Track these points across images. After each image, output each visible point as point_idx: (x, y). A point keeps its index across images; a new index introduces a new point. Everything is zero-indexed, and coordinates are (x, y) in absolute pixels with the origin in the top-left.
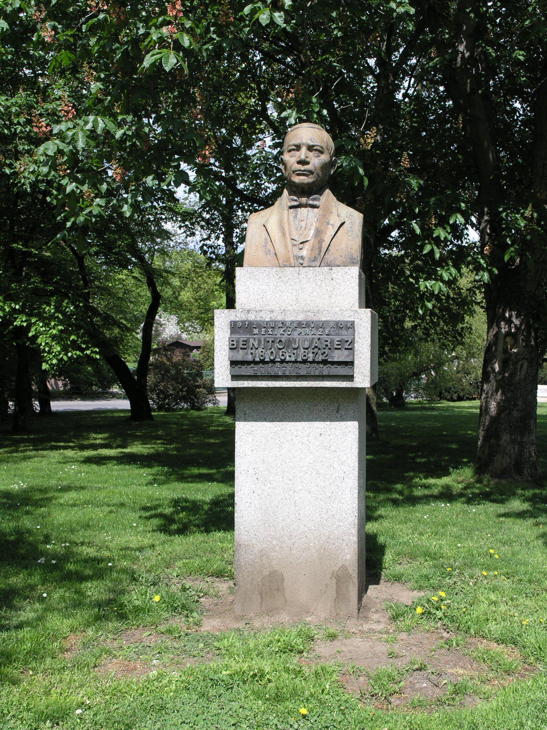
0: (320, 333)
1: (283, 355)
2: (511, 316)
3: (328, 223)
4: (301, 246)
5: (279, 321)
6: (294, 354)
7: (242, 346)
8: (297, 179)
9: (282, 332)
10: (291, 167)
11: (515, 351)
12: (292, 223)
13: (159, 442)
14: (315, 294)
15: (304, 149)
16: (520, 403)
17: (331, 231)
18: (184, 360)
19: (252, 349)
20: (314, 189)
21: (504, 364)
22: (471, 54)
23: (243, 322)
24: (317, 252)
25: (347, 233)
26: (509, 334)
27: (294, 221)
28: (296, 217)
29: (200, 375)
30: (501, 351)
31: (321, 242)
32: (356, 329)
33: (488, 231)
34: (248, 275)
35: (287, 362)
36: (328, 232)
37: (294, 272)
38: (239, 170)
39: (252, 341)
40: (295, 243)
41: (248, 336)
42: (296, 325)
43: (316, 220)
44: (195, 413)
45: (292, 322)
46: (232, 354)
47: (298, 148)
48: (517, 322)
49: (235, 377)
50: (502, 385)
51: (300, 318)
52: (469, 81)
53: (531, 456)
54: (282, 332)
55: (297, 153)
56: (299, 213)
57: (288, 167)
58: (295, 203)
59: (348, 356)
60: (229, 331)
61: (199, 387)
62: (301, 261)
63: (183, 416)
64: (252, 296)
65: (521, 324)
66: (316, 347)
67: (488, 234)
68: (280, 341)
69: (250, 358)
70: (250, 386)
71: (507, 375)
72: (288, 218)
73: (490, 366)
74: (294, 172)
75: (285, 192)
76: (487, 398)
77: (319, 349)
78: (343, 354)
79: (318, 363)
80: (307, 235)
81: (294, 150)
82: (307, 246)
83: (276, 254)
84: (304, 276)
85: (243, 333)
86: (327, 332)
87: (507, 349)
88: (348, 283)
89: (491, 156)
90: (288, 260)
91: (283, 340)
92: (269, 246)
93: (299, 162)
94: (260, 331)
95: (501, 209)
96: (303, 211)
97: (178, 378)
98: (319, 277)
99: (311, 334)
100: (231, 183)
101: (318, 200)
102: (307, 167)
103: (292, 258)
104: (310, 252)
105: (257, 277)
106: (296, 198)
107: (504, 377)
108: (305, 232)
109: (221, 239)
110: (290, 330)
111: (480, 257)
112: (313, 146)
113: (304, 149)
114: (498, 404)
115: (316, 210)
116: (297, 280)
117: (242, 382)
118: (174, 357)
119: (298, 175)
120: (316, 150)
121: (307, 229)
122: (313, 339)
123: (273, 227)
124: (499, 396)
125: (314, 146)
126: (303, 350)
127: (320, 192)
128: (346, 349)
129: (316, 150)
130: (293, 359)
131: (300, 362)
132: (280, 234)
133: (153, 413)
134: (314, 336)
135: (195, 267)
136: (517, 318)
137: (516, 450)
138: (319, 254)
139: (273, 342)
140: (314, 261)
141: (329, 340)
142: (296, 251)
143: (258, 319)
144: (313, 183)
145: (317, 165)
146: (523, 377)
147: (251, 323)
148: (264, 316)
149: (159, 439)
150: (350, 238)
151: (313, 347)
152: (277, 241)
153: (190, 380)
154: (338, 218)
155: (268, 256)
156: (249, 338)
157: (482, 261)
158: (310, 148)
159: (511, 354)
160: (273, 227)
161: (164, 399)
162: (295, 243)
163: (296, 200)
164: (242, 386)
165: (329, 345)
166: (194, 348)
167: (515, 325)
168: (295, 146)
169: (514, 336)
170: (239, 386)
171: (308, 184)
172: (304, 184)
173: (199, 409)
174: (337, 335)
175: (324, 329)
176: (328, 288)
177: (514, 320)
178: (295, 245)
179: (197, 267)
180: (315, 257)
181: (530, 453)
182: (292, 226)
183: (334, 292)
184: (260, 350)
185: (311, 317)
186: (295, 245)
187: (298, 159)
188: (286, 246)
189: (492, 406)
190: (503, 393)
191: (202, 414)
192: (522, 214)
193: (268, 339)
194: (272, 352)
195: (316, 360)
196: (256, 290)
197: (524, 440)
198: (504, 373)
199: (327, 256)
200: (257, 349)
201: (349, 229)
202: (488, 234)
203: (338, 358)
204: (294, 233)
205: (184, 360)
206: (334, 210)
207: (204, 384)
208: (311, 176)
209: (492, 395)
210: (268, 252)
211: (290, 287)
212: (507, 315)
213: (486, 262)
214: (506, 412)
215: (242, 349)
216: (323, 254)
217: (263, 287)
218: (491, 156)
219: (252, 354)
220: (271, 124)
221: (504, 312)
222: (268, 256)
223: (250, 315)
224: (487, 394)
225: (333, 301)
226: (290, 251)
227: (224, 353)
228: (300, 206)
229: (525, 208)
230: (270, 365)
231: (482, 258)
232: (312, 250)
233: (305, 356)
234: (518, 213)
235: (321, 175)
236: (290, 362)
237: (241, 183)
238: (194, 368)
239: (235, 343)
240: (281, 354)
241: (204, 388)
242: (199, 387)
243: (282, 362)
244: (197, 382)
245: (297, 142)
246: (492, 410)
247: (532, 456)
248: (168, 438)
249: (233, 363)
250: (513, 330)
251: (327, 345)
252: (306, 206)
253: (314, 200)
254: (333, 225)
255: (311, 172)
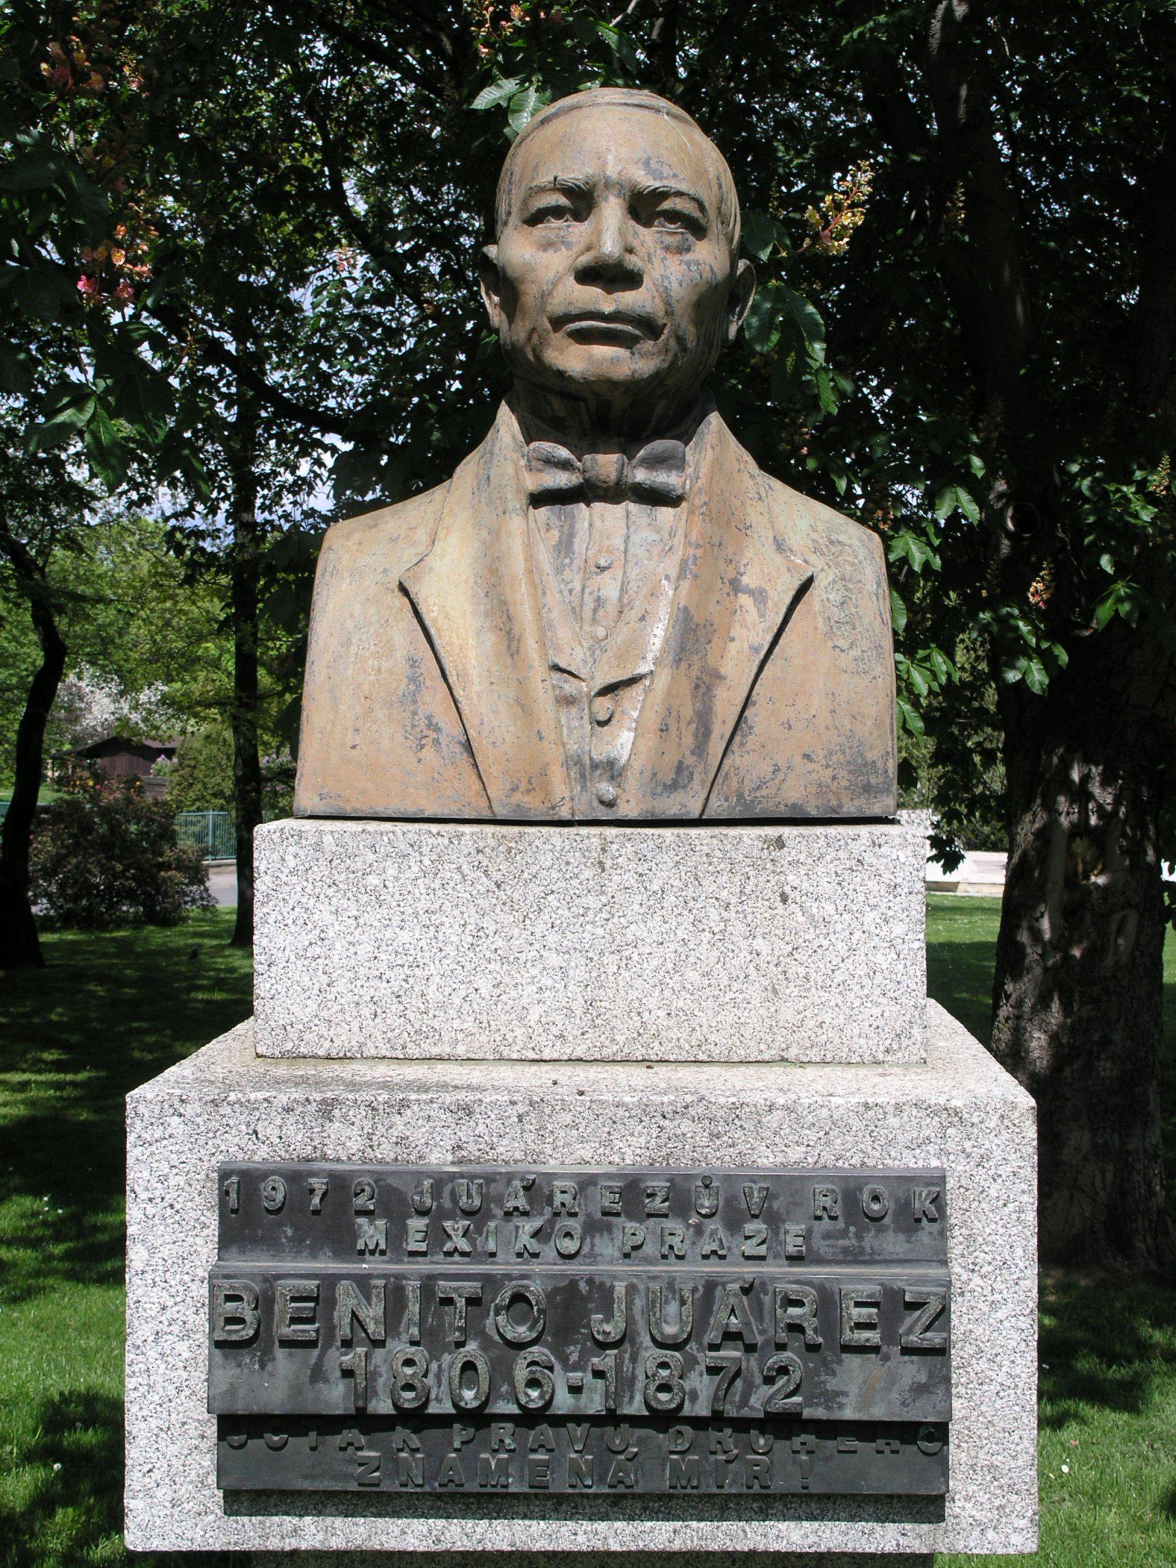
0: (749, 1248)
1: (533, 1383)
2: (1085, 779)
3: (735, 586)
4: (603, 706)
5: (510, 1177)
6: (599, 1374)
7: (287, 1331)
8: (575, 360)
9: (525, 1239)
10: (544, 296)
11: (1101, 880)
12: (552, 581)
13: (48, 1056)
14: (692, 976)
15: (611, 212)
16: (1117, 1037)
17: (751, 628)
18: (129, 801)
19: (347, 1344)
20: (659, 409)
21: (1071, 917)
22: (971, 9)
23: (296, 1178)
24: (689, 741)
25: (830, 635)
26: (1080, 829)
27: (559, 570)
28: (565, 546)
29: (169, 836)
30: (1061, 882)
31: (705, 685)
32: (954, 1216)
33: (1010, 526)
34: (320, 870)
35: (560, 1421)
36: (736, 632)
37: (575, 858)
38: (270, 338)
39: (347, 1299)
40: (570, 687)
41: (327, 1265)
42: (608, 1201)
43: (671, 566)
44: (156, 936)
45: (586, 1183)
46: (228, 1373)
47: (581, 201)
48: (1105, 797)
49: (240, 1499)
50: (1060, 982)
51: (631, 1150)
52: (963, 92)
53: (1151, 1193)
54: (525, 1239)
55: (578, 231)
56: (582, 525)
57: (530, 293)
58: (562, 480)
59: (920, 1390)
60: (213, 1220)
61: (167, 866)
62: (608, 789)
63: (124, 947)
64: (341, 986)
65: (1117, 802)
66: (730, 1336)
67: (1009, 535)
68: (519, 1298)
69: (335, 1397)
70: (336, 1543)
71: (1077, 953)
72: (530, 557)
73: (1025, 924)
74: (558, 322)
75: (507, 421)
76: (1018, 1017)
77: (750, 1348)
78: (892, 1379)
79: (742, 1425)
80: (634, 648)
81: (557, 212)
82: (632, 702)
83: (468, 746)
84: (631, 879)
85: (297, 1245)
86: (792, 1244)
87: (1076, 873)
88: (870, 917)
89: (1019, 308)
90: (538, 781)
91: (536, 1289)
92: (434, 701)
93: (589, 275)
94: (396, 1235)
95: (1075, 468)
96: (604, 519)
97: (114, 845)
98: (709, 887)
99: (691, 1258)
100: (248, 369)
101: (673, 462)
102: (628, 299)
103: (557, 774)
104: (650, 741)
105: (373, 880)
106: (563, 453)
107: (1068, 957)
108: (623, 633)
109: (221, 517)
110: (575, 1225)
111: (1016, 612)
112: (660, 195)
113: (611, 212)
114: (1054, 1039)
115: (665, 513)
116: (592, 901)
117: (289, 1521)
118: (105, 794)
119: (584, 337)
120: (673, 216)
121: (632, 615)
122: (711, 1286)
123: (450, 596)
124: (1055, 1014)
125: (663, 195)
126: (651, 1355)
127: (682, 424)
128: (907, 1351)
129: (673, 216)
130: (594, 1403)
131: (635, 1421)
132: (490, 639)
133: (45, 938)
134: (712, 1268)
135: (156, 573)
136: (1104, 784)
137: (1109, 1176)
138: (700, 749)
139: (472, 1301)
140: (673, 787)
141: (810, 1296)
142: (574, 731)
143: (386, 1151)
144: (657, 377)
145: (677, 291)
146: (1125, 959)
147: (341, 1185)
148: (418, 1136)
149: (47, 1045)
150: (845, 660)
151: (713, 1336)
152: (474, 674)
153: (145, 851)
154: (778, 559)
155: (428, 753)
156: (330, 1281)
157: (1023, 627)
158: (644, 206)
159: (1088, 891)
160: (450, 596)
161: (76, 899)
162: (570, 687)
163: (565, 465)
164: (289, 1544)
165: (810, 1325)
166: (159, 752)
167: (1100, 808)
168: (569, 191)
169: (1097, 837)
170: (274, 1544)
171: (633, 387)
172: (613, 384)
173: (167, 920)
174: (854, 1257)
175: (774, 1220)
176: (759, 944)
177: (1096, 790)
178: (568, 701)
179: (161, 574)
180: (680, 768)
181: (1149, 1184)
182: (552, 599)
183: (795, 969)
184: (400, 1348)
185: (699, 1151)
186: (568, 701)
187: (585, 259)
188: (523, 706)
189: (1034, 1044)
190: (1066, 1009)
191: (173, 937)
192: (1142, 485)
193: (444, 1287)
194: (469, 1366)
195: (731, 1411)
196: (365, 950)
197: (1130, 1147)
198: (1070, 944)
199: (736, 758)
200: (380, 1344)
201: (837, 614)
202: (1009, 535)
203: (865, 1401)
204: (564, 633)
205: (129, 801)
206: (755, 515)
207: (179, 860)
208: (648, 345)
209: (1034, 1009)
210: (425, 734)
211: (553, 938)
212: (1075, 776)
213: (1036, 631)
214: (1078, 1065)
215: (287, 1343)
216: (716, 747)
217: (405, 936)
218: (1019, 308)
219: (348, 1373)
220: (351, 223)
221: (1066, 768)
222: (428, 753)
223: (335, 1129)
224: (1019, 1004)
225: (788, 1014)
226: (549, 733)
227: (183, 1347)
228: (587, 492)
229: (1152, 465)
230: (459, 1435)
231: (1025, 617)
232: (664, 729)
233: (664, 1387)
234: (1129, 483)
235: (691, 341)
236: (578, 1419)
237: (274, 369)
238: (153, 821)
239: (246, 1310)
240: (521, 1373)
241: (178, 868)
242: (167, 866)
243: (528, 1418)
244: (161, 855)
245: (575, 173)
246: (1036, 1054)
247: (1155, 1194)
248: (75, 1039)
249: (235, 1426)
250: (1093, 820)
251: (795, 1328)
252: (615, 493)
253: (654, 462)
254: (759, 596)
255: (649, 327)
